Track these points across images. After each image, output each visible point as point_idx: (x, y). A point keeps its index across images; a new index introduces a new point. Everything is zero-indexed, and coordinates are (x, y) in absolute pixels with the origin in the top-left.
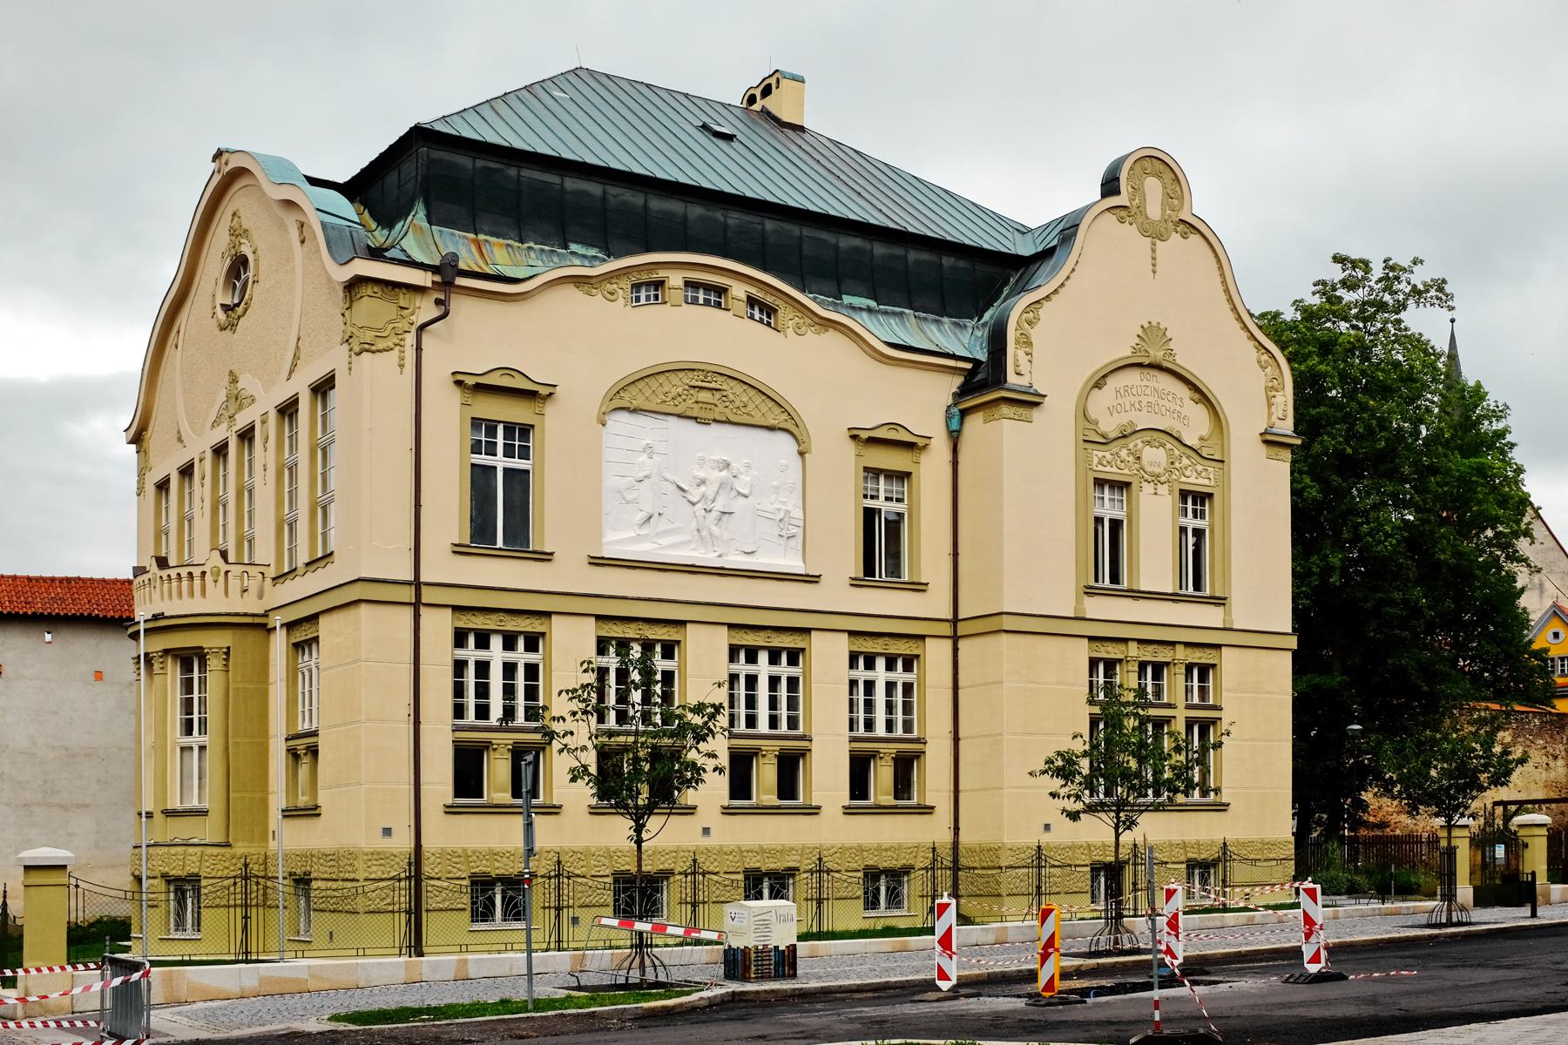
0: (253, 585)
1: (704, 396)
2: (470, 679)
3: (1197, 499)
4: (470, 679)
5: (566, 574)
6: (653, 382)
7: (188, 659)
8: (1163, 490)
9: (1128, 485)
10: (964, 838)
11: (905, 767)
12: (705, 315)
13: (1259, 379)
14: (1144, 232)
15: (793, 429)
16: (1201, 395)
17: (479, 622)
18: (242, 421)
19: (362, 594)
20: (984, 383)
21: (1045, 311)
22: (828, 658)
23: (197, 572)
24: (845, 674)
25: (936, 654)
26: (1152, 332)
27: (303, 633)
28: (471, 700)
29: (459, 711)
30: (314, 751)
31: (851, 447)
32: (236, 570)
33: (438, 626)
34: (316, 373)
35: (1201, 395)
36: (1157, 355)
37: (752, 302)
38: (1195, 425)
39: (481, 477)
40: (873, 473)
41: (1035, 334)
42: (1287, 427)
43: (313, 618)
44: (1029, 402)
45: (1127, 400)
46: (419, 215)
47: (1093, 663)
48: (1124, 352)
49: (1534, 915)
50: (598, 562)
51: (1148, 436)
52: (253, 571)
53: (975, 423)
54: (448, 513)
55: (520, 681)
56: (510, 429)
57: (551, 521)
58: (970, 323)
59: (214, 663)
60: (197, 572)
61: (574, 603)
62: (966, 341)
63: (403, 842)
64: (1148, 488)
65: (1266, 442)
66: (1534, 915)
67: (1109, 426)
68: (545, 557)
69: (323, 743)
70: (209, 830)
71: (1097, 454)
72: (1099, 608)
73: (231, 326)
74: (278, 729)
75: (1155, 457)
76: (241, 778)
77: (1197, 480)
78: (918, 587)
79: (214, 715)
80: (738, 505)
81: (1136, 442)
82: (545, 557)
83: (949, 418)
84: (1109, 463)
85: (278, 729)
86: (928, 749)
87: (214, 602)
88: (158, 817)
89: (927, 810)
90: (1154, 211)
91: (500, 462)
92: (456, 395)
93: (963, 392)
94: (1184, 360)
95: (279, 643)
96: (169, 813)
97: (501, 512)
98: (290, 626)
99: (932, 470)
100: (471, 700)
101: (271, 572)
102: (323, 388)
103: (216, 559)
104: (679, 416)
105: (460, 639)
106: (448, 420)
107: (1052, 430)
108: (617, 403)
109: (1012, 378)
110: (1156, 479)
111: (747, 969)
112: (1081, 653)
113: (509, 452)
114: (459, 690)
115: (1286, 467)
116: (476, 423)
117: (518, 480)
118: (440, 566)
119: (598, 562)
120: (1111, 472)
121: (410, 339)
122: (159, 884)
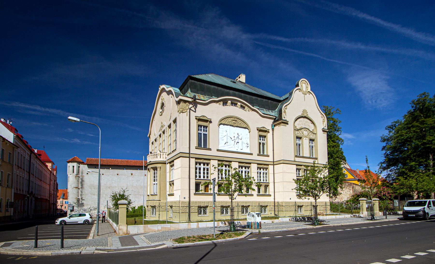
0: (164, 156)
1: (234, 122)
2: (198, 171)
3: (312, 140)
4: (198, 171)
5: (213, 152)
6: (226, 119)
7: (155, 169)
8: (307, 139)
9: (301, 138)
10: (276, 201)
11: (266, 186)
12: (233, 107)
13: (321, 120)
14: (303, 94)
15: (247, 127)
16: (313, 123)
17: (199, 161)
18: (163, 130)
19: (181, 155)
20: (279, 120)
21: (288, 107)
22: (254, 167)
23: (156, 154)
24: (256, 171)
25: (271, 167)
26: (304, 111)
27: (172, 163)
28: (198, 175)
29: (196, 177)
30: (173, 184)
31: (257, 132)
32: (162, 153)
33: (193, 161)
34: (173, 119)
35: (313, 123)
36: (305, 115)
37: (241, 106)
38: (312, 127)
39: (199, 135)
40: (260, 136)
41: (286, 110)
42: (326, 128)
43: (173, 161)
44: (286, 123)
45: (301, 123)
46: (189, 91)
47: (297, 169)
48: (300, 114)
49: (386, 218)
50: (218, 150)
51: (304, 129)
52: (164, 154)
53: (276, 128)
54: (194, 143)
55: (206, 171)
56: (204, 127)
57: (211, 144)
58: (274, 111)
59: (158, 169)
60: (156, 154)
61: (214, 158)
62: (274, 113)
63: (187, 200)
64: (305, 138)
65: (323, 131)
66: (386, 218)
67: (298, 127)
68: (210, 149)
69: (174, 182)
70: (157, 198)
71: (297, 132)
72: (297, 159)
73: (161, 115)
74: (168, 180)
75: (306, 133)
76: (162, 189)
77: (312, 137)
78: (268, 156)
79: (158, 178)
80: (240, 141)
81: (303, 130)
82: (210, 149)
83: (272, 126)
84: (299, 134)
85: (168, 180)
86: (270, 184)
87: (159, 159)
88: (150, 196)
89: (270, 195)
90: (304, 89)
91: (202, 132)
92: (196, 121)
93: (274, 122)
94: (310, 116)
95: (168, 166)
96: (152, 195)
97: (203, 142)
98: (170, 163)
99: (269, 136)
100: (198, 175)
101: (167, 154)
102: (175, 121)
103: (159, 152)
104: (230, 125)
105: (196, 163)
106: (194, 123)
107: (290, 128)
108: (221, 123)
109: (283, 118)
110: (306, 137)
111: (252, 227)
112: (295, 167)
113: (204, 131)
114: (196, 173)
115: (326, 135)
116: (199, 126)
117: (205, 135)
118: (194, 151)
119: (218, 150)
120: (299, 135)
121: (188, 110)
122: (150, 207)
